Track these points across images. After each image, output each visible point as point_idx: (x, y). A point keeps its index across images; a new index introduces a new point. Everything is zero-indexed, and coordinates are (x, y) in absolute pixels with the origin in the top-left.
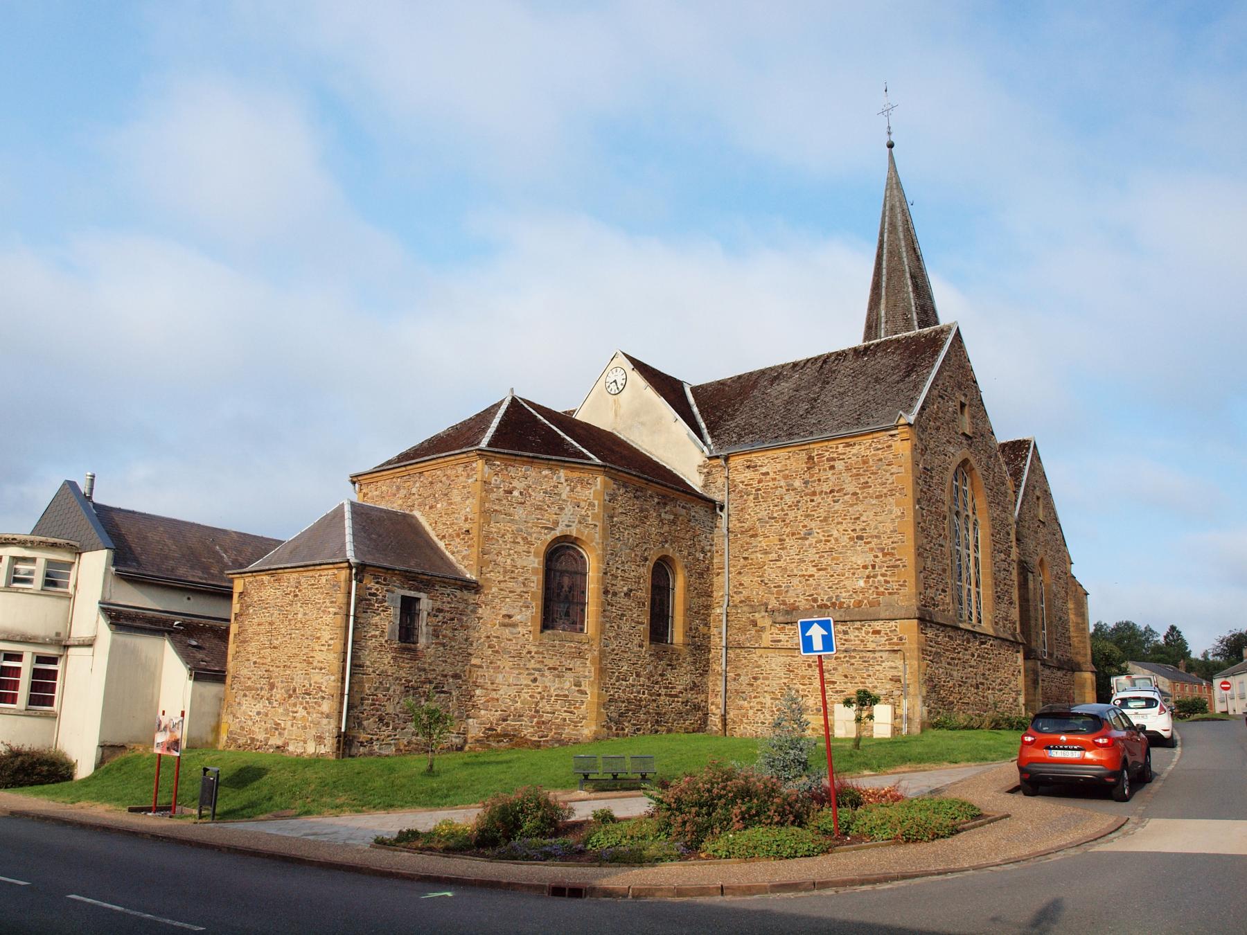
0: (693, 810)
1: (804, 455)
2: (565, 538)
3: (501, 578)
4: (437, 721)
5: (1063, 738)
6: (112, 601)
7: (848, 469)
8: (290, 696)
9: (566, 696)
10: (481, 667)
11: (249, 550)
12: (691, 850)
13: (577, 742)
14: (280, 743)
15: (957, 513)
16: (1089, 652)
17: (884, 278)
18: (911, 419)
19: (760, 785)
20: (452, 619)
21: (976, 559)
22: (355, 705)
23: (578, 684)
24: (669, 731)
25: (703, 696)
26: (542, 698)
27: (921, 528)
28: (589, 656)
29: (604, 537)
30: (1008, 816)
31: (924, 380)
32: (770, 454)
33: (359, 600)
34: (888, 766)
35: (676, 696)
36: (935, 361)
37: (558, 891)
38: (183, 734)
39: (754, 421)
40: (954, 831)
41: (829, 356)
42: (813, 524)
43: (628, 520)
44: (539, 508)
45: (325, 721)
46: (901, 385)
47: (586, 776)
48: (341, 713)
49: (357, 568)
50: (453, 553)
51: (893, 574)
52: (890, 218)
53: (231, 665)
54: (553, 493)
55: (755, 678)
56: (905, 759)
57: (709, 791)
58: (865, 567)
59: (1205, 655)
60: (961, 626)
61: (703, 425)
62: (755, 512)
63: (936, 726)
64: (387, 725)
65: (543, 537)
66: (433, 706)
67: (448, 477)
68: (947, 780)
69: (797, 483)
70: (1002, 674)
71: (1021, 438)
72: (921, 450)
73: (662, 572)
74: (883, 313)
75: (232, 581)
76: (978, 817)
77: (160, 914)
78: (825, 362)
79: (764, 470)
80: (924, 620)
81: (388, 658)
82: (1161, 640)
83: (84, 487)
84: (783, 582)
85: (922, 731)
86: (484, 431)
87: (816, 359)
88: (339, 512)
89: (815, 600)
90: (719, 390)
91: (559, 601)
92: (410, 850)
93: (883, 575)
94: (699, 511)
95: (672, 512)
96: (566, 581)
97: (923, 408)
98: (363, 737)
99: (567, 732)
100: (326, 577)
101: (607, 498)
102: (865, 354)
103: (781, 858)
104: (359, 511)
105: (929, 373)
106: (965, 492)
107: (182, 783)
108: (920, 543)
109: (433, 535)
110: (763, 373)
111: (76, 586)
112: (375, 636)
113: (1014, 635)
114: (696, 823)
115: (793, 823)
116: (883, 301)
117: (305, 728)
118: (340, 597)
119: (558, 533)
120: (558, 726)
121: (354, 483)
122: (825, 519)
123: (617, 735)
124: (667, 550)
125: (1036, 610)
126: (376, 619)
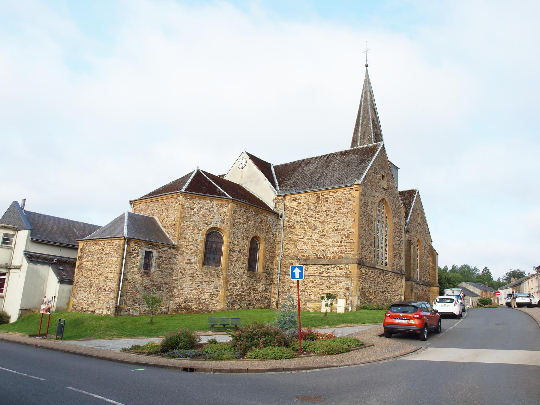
0: (245, 340)
1: (316, 196)
2: (214, 228)
3: (187, 244)
4: (156, 302)
5: (401, 315)
6: (29, 251)
7: (333, 202)
8: (98, 291)
9: (211, 293)
10: (177, 280)
11: (86, 231)
12: (242, 355)
13: (214, 312)
14: (93, 310)
15: (379, 221)
16: (437, 278)
17: (361, 121)
18: (360, 182)
19: (272, 331)
20: (166, 261)
21: (386, 240)
22: (123, 293)
23: (216, 288)
24: (254, 308)
25: (269, 294)
26: (201, 293)
27: (361, 227)
28: (221, 276)
29: (231, 228)
30: (373, 345)
31: (367, 166)
32: (302, 195)
33: (128, 252)
34: (336, 325)
35: (258, 294)
36: (372, 158)
37: (185, 369)
38: (54, 306)
39: (297, 181)
40: (348, 351)
41: (330, 155)
42: (318, 224)
43: (242, 222)
44: (204, 216)
45: (111, 301)
46: (357, 168)
47: (213, 326)
48: (117, 298)
49: (128, 240)
50: (168, 234)
51: (349, 246)
52: (365, 96)
53: (76, 277)
54: (211, 210)
55: (291, 287)
56: (344, 322)
57: (252, 332)
58: (338, 242)
59: (499, 280)
60: (377, 267)
61: (277, 182)
62: (295, 219)
63: (362, 308)
64: (136, 303)
65: (205, 228)
66: (155, 295)
67: (168, 203)
68: (357, 330)
69: (312, 207)
70: (394, 287)
71: (412, 189)
72: (363, 194)
73: (254, 242)
74: (359, 135)
75: (78, 243)
76: (361, 345)
77: (30, 374)
78: (328, 157)
79: (299, 201)
80: (361, 264)
81: (138, 276)
82: (481, 273)
83: (21, 204)
84: (304, 247)
85: (357, 310)
86: (184, 184)
87: (325, 156)
88: (122, 218)
89: (317, 255)
90: (285, 167)
91: (211, 252)
92: (134, 353)
93: (345, 246)
94: (272, 218)
95: (260, 218)
96: (214, 245)
97: (365, 177)
98: (126, 307)
99: (211, 307)
100: (115, 243)
101: (233, 212)
102: (345, 154)
103: (276, 359)
104: (131, 216)
105: (369, 163)
106: (383, 212)
107: (52, 325)
108: (360, 233)
109: (161, 226)
110: (303, 161)
111: (15, 244)
112: (134, 267)
113: (401, 271)
114: (246, 345)
115: (284, 346)
116: (360, 130)
117: (103, 304)
118: (120, 251)
119: (211, 226)
120: (207, 305)
121: (131, 204)
122: (323, 222)
123: (232, 309)
124: (257, 234)
125: (414, 260)
126: (134, 260)
